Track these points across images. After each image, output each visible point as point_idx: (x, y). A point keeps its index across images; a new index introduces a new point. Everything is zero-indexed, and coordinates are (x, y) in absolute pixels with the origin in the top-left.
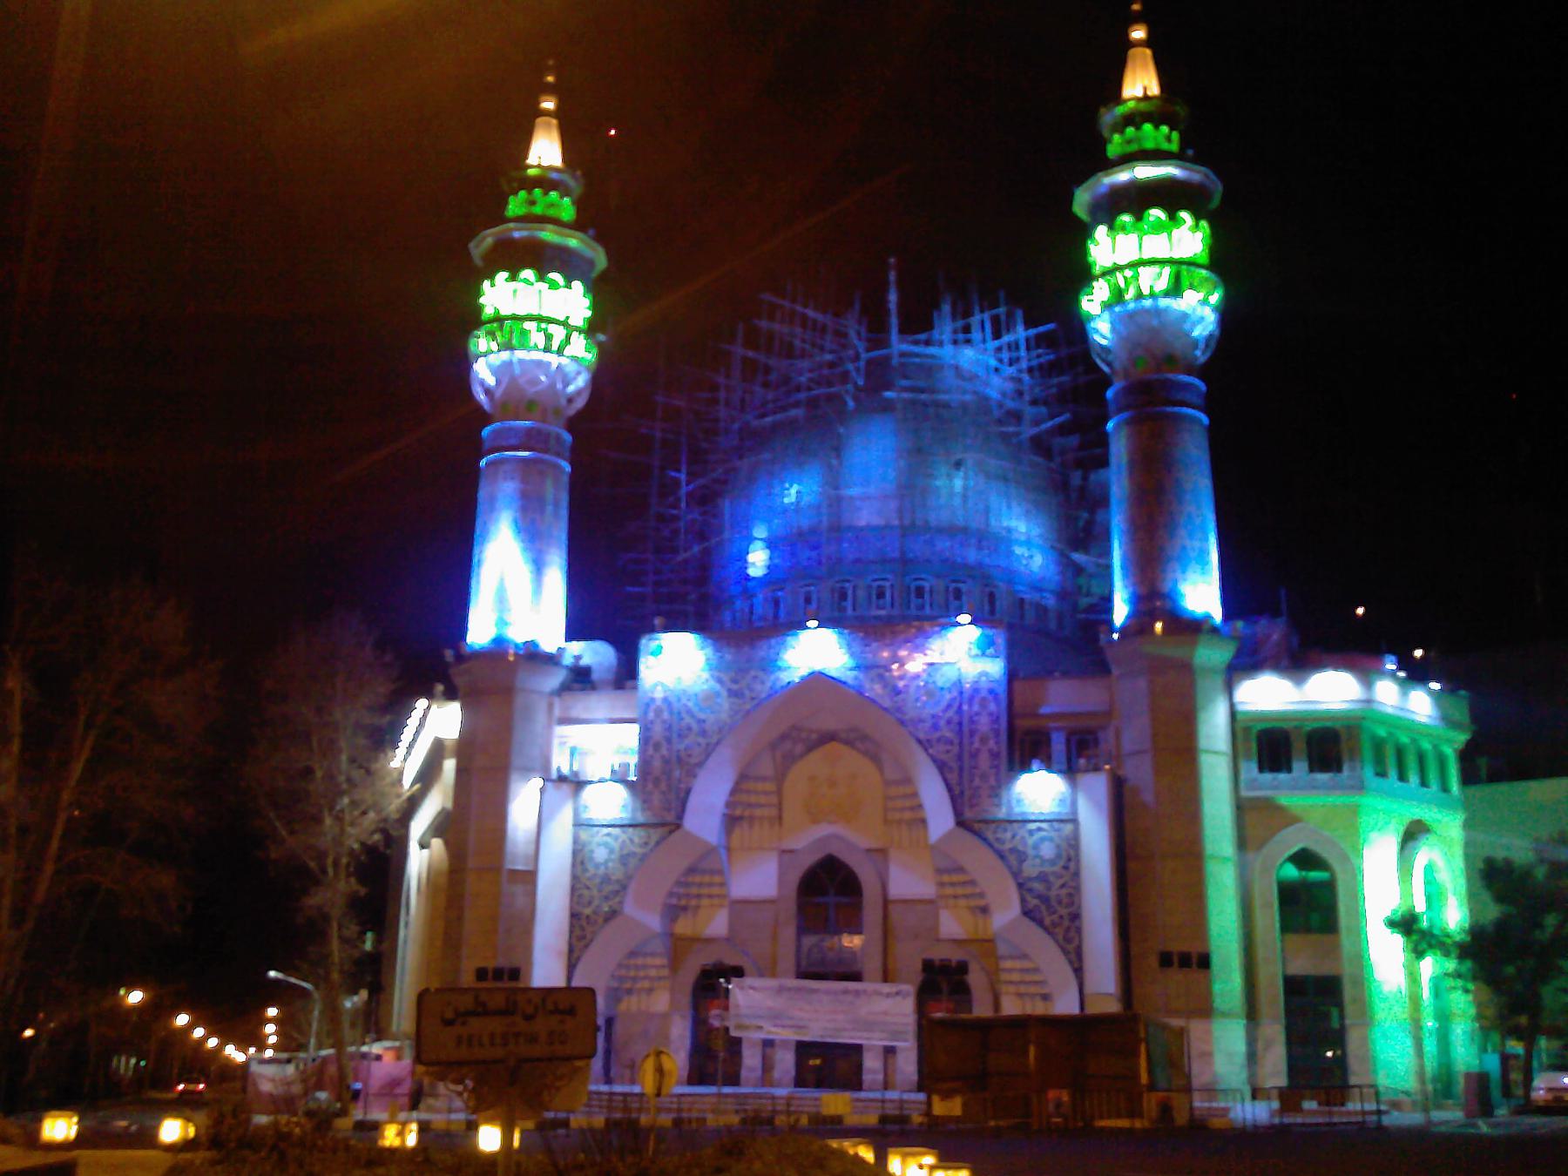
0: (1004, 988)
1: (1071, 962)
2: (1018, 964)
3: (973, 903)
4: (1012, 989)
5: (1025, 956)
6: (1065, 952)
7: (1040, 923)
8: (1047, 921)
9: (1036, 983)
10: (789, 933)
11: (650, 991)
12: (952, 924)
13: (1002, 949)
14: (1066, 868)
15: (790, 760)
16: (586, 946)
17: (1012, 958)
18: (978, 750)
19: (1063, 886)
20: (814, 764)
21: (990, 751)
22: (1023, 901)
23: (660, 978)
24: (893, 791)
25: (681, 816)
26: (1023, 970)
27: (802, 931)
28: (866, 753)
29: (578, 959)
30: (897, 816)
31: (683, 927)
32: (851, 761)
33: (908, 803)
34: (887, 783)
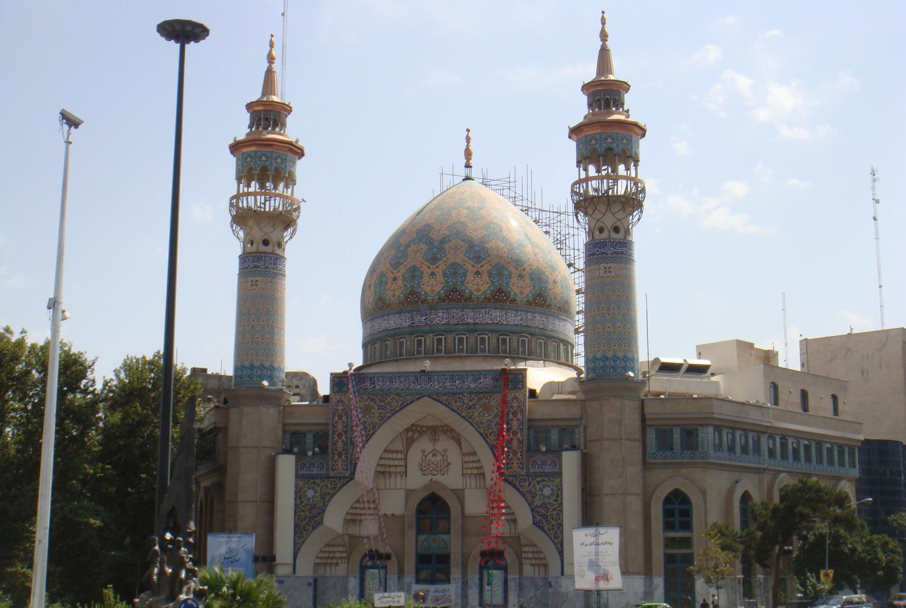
0: (524, 561)
1: (557, 549)
2: (531, 549)
3: (509, 517)
4: (528, 561)
5: (535, 545)
6: (555, 544)
7: (542, 529)
8: (546, 528)
9: (540, 559)
10: (411, 535)
11: (337, 564)
12: (500, 528)
13: (523, 541)
14: (556, 500)
15: (410, 442)
16: (303, 542)
17: (528, 546)
18: (337, 441)
19: (554, 510)
20: (424, 444)
21: (343, 441)
22: (534, 517)
23: (342, 558)
24: (467, 459)
25: (353, 474)
26: (533, 552)
27: (419, 531)
28: (453, 438)
29: (299, 549)
30: (469, 471)
31: (354, 530)
32: (445, 444)
33: (475, 465)
34: (464, 455)
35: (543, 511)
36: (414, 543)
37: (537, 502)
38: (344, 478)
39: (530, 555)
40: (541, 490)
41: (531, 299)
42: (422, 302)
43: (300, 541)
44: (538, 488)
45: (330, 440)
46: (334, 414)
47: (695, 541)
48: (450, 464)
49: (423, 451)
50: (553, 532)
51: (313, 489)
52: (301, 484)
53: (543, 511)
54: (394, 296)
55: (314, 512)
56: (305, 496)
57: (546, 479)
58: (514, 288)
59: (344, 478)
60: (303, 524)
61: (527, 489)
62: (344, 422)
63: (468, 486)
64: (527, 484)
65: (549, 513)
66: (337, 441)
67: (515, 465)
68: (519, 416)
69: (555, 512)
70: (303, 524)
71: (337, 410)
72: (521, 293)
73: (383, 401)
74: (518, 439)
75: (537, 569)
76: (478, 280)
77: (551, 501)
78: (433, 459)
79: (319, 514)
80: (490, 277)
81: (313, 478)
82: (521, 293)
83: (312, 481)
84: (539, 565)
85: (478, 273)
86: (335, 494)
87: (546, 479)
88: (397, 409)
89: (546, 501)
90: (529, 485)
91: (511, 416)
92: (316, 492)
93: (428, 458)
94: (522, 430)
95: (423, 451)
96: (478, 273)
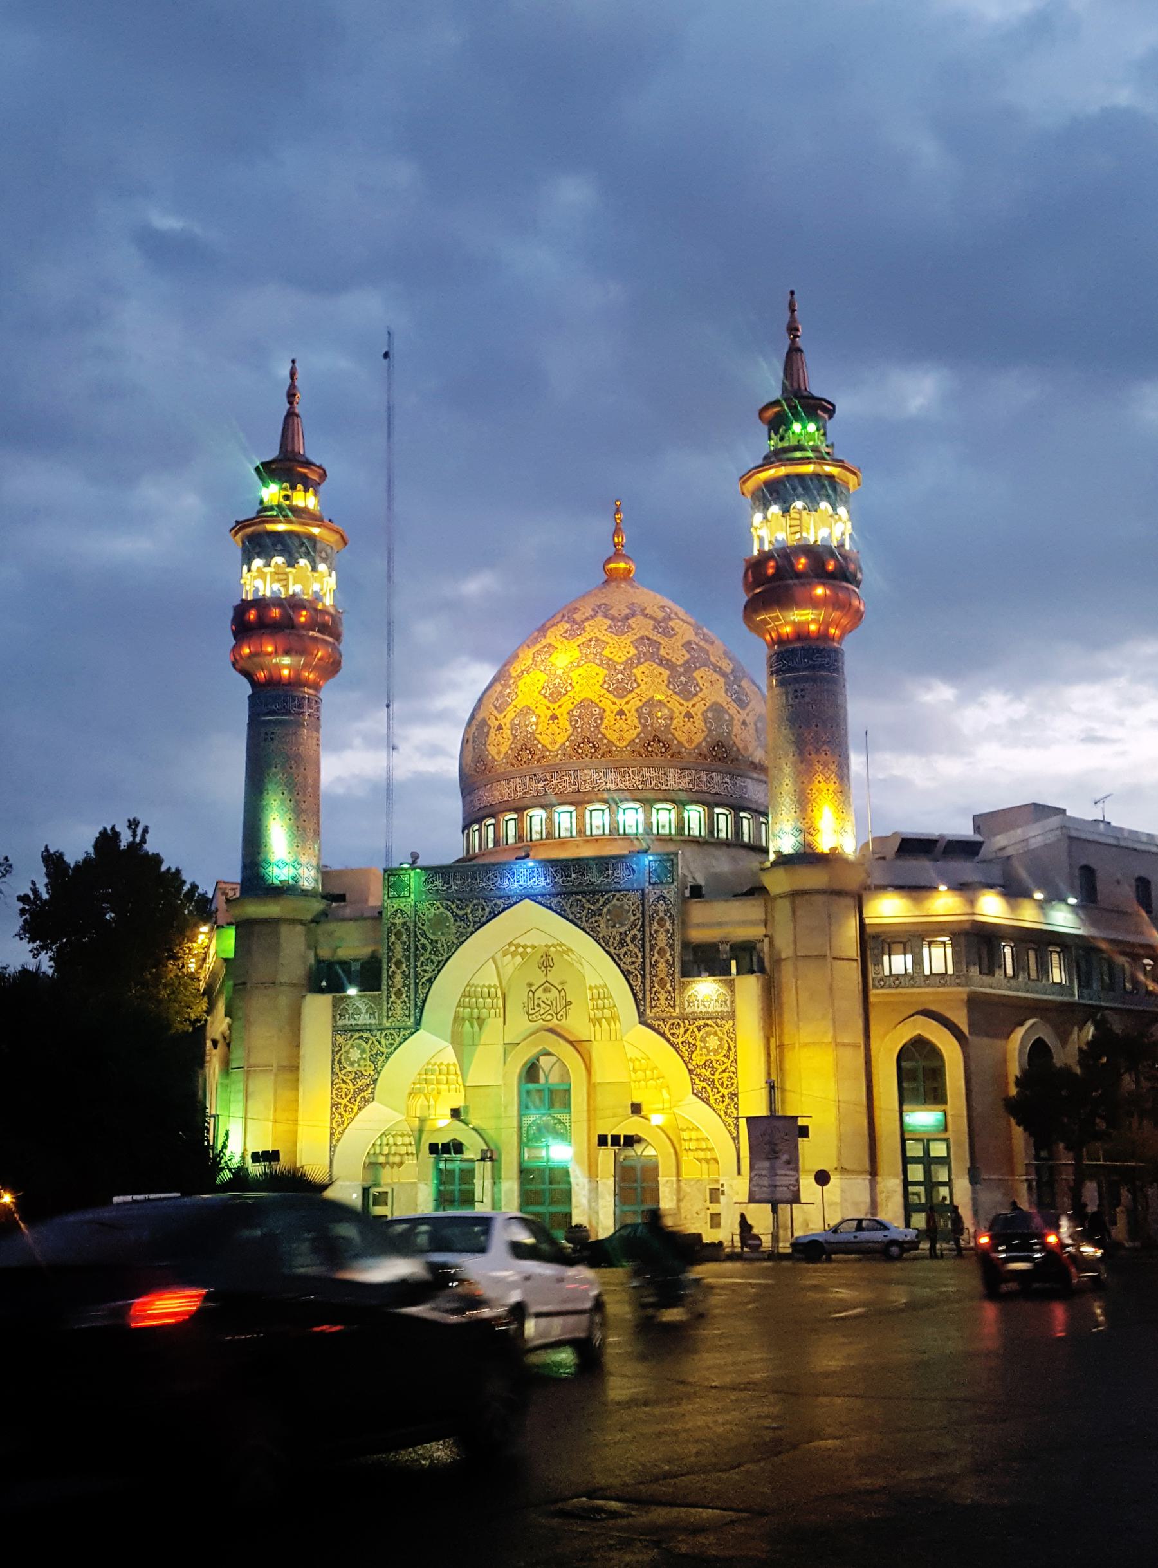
8: (712, 1102)
18: (657, 961)
21: (667, 961)
22: (693, 1083)
35: (706, 1073)
36: (515, 1124)
37: (698, 1059)
39: (693, 1145)
40: (703, 1040)
42: (732, 761)
43: (340, 1129)
45: (385, 971)
46: (390, 931)
47: (614, 1132)
49: (530, 985)
50: (722, 1106)
51: (359, 1047)
52: (340, 1039)
53: (706, 1073)
54: (499, 753)
55: (361, 1082)
56: (347, 1059)
57: (710, 1022)
60: (344, 1102)
61: (681, 1040)
63: (598, 1037)
64: (682, 1030)
65: (716, 1077)
66: (657, 961)
67: (663, 1001)
69: (726, 1075)
70: (344, 1102)
71: (394, 924)
73: (461, 909)
74: (667, 961)
75: (705, 1165)
77: (719, 1057)
78: (544, 997)
80: (639, 718)
81: (359, 1031)
83: (357, 1035)
84: (707, 1161)
85: (621, 713)
86: (392, 1053)
87: (710, 1022)
88: (484, 919)
90: (685, 1032)
91: (655, 926)
92: (364, 1051)
93: (536, 995)
94: (672, 946)
96: (621, 713)
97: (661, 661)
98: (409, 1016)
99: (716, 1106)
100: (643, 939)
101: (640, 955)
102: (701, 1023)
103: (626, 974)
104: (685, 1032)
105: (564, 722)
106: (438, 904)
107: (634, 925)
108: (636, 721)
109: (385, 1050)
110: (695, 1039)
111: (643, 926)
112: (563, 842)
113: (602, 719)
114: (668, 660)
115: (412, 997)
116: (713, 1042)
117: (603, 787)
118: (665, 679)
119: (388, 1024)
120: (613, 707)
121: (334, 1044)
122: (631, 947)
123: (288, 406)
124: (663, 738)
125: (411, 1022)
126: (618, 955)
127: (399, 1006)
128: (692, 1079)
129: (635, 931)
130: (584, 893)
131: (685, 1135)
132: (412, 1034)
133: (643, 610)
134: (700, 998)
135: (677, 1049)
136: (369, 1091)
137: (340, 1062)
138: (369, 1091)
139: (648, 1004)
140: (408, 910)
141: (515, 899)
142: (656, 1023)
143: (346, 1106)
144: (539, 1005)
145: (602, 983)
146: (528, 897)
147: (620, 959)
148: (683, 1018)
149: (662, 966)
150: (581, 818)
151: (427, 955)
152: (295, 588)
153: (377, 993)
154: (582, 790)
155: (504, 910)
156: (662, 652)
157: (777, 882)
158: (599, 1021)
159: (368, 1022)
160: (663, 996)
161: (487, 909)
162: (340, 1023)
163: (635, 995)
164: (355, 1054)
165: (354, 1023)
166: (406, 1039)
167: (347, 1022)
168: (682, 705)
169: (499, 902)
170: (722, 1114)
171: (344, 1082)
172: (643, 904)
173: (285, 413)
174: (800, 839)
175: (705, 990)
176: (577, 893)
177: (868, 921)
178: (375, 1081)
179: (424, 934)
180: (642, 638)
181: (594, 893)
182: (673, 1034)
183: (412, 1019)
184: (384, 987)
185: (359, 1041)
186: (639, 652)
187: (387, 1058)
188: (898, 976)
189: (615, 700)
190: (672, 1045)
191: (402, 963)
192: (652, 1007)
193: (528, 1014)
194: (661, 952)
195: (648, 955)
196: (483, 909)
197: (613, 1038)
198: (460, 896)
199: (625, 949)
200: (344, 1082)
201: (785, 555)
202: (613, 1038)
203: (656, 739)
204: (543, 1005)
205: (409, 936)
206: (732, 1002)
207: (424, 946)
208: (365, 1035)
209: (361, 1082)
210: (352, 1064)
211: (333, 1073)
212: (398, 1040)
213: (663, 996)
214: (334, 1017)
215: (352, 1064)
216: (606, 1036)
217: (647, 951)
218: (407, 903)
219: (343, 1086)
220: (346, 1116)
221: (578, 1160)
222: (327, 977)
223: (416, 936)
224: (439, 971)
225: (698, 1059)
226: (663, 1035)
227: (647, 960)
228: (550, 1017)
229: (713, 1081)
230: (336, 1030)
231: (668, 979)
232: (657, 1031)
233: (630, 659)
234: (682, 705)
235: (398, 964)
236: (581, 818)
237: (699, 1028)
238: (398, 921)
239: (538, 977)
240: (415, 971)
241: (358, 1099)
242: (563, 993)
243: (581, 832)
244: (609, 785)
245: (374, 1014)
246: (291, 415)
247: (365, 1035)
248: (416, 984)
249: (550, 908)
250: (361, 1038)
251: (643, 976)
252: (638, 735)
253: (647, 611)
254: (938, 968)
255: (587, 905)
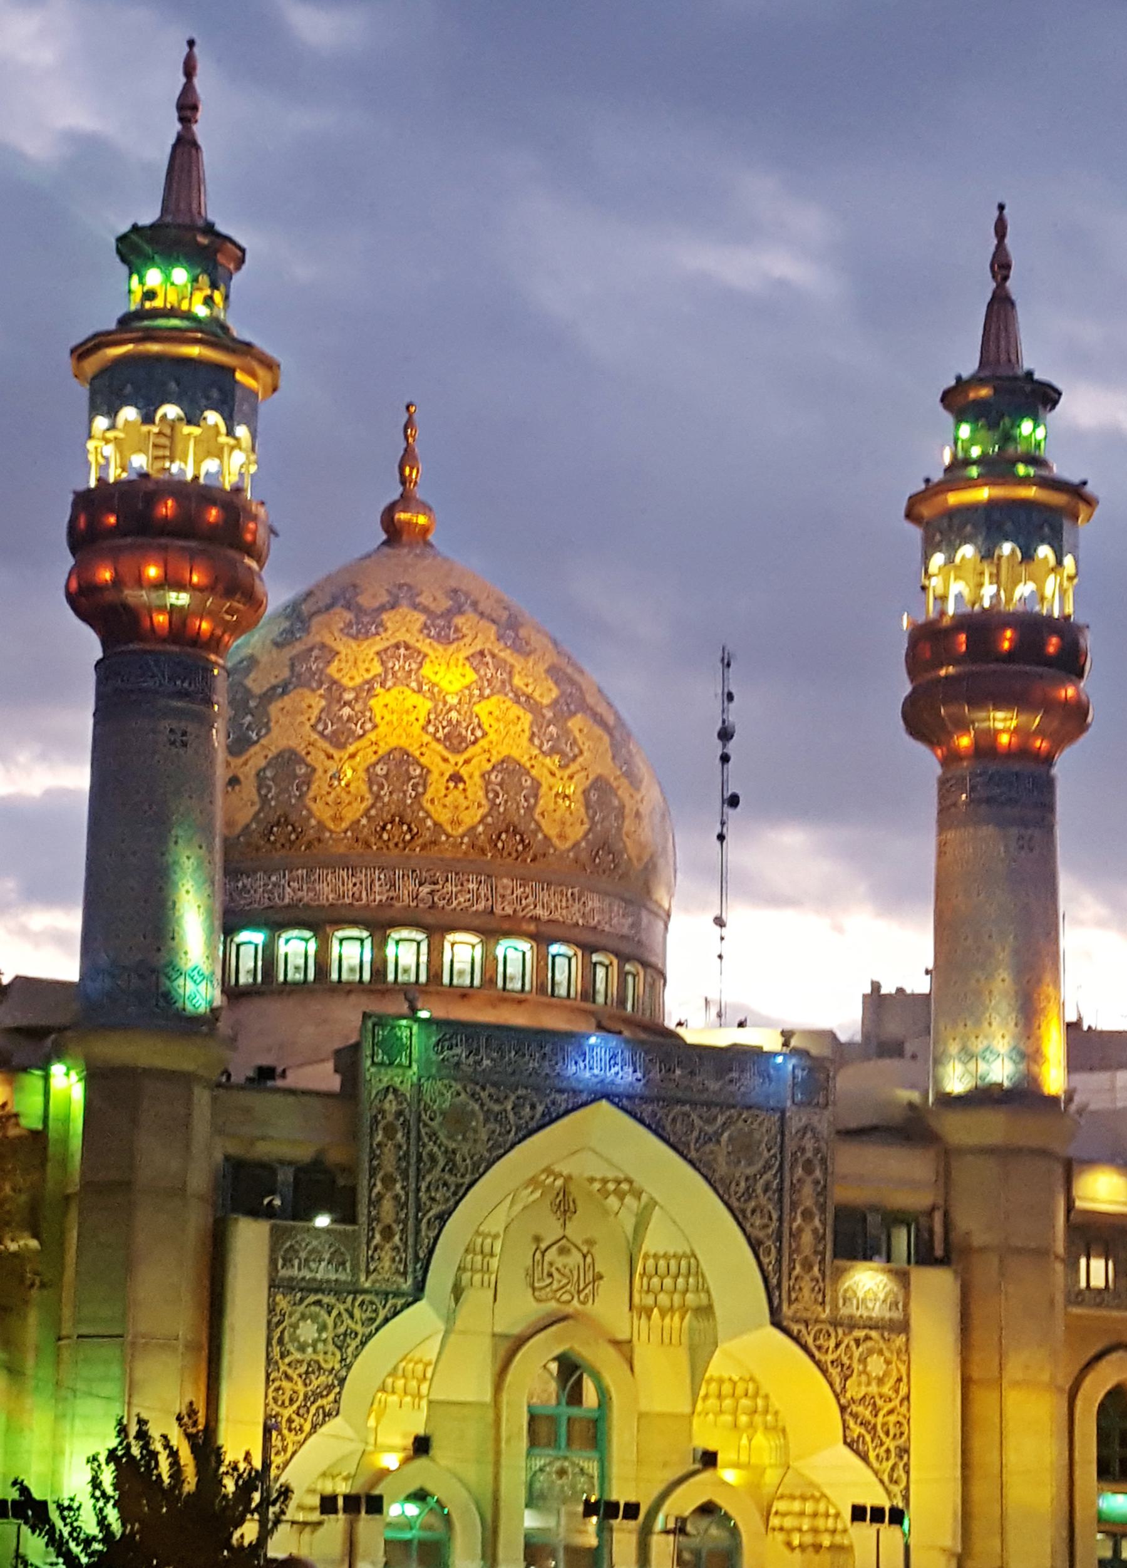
8: (872, 1455)
18: (800, 1230)
19: (891, 1412)
21: (396, 1197)
22: (845, 1427)
35: (866, 1413)
38: (397, 1294)
40: (863, 1360)
41: (584, 856)
44: (856, 1354)
46: (375, 1121)
48: (601, 1277)
51: (314, 1318)
52: (283, 1302)
55: (319, 1381)
56: (294, 1339)
58: (544, 823)
59: (397, 1294)
60: (287, 1413)
61: (830, 1357)
62: (817, 1182)
64: (832, 1343)
65: (880, 1419)
66: (800, 1230)
68: (818, 1173)
69: (892, 1419)
70: (287, 1413)
71: (382, 1111)
72: (562, 836)
73: (497, 1101)
74: (396, 1197)
76: (456, 795)
79: (330, 1388)
81: (316, 1291)
82: (562, 836)
85: (456, 778)
86: (370, 1336)
88: (533, 1125)
89: (874, 1389)
90: (837, 1346)
92: (323, 1328)
93: (547, 1258)
95: (537, 1239)
96: (456, 778)
97: (516, 695)
98: (404, 1274)
99: (876, 1465)
100: (780, 1190)
101: (775, 1216)
102: (860, 1334)
103: (755, 1245)
104: (837, 1346)
105: (475, 789)
106: (459, 1087)
107: (767, 1167)
108: (481, 793)
109: (359, 1328)
110: (850, 1358)
111: (781, 1167)
112: (506, 998)
113: (536, 796)
114: (528, 697)
115: (410, 1242)
116: (875, 1365)
117: (530, 912)
118: (527, 727)
119: (367, 1285)
120: (443, 765)
121: (271, 1310)
122: (763, 1200)
123: (178, 126)
124: (522, 828)
125: (407, 1285)
126: (743, 1211)
127: (387, 1255)
128: (844, 1421)
129: (768, 1176)
130: (694, 1104)
131: (779, 1506)
132: (408, 1305)
133: (475, 604)
134: (860, 1295)
135: (824, 1372)
136: (331, 1397)
137: (281, 1341)
138: (331, 1397)
139: (785, 1296)
140: (406, 1089)
141: (584, 1097)
142: (795, 1328)
143: (290, 1420)
144: (550, 1275)
145: (681, 1248)
146: (608, 1096)
147: (744, 1216)
148: (836, 1323)
149: (807, 1238)
150: (435, 952)
151: (437, 1172)
152: (185, 468)
153: (349, 1228)
154: (498, 910)
155: (567, 1112)
156: (517, 681)
157: (958, 1129)
158: (649, 1312)
159: (333, 1277)
160: (806, 1285)
161: (540, 1109)
162: (283, 1273)
163: (766, 1280)
164: (307, 1331)
165: (309, 1276)
166: (396, 1314)
167: (294, 1272)
168: (446, 760)
169: (561, 1098)
170: (886, 1478)
171: (288, 1378)
172: (783, 1134)
173: (172, 140)
174: (1022, 1067)
175: (868, 1283)
176: (683, 1102)
177: (1079, 1204)
178: (342, 1381)
179: (433, 1136)
180: (482, 653)
181: (709, 1104)
182: (819, 1348)
183: (410, 1281)
184: (363, 1219)
185: (316, 1309)
186: (481, 678)
187: (363, 1344)
188: (1099, 1291)
189: (446, 754)
190: (818, 1363)
191: (395, 1181)
192: (790, 1302)
193: (534, 1289)
194: (807, 1215)
195: (786, 1217)
196: (533, 1107)
197: (667, 1340)
198: (495, 1077)
199: (753, 1204)
200: (288, 1378)
201: (980, 626)
202: (667, 1340)
203: (513, 829)
204: (556, 1275)
205: (407, 1135)
206: (906, 1306)
207: (433, 1158)
208: (326, 1300)
209: (319, 1381)
210: (302, 1348)
211: (269, 1360)
212: (382, 1314)
213: (806, 1285)
214: (273, 1262)
215: (302, 1348)
216: (655, 1337)
217: (787, 1209)
218: (407, 1078)
219: (286, 1384)
220: (291, 1438)
221: (26, 1540)
222: (246, 1187)
223: (419, 1137)
224: (457, 1203)
225: (854, 1390)
226: (805, 1348)
227: (786, 1225)
228: (566, 1297)
229: (875, 1427)
230: (274, 1285)
231: (397, 1228)
232: (796, 1339)
233: (468, 687)
234: (446, 760)
235: (388, 1181)
236: (435, 952)
237: (858, 1342)
238: (391, 1106)
239: (552, 1229)
240: (418, 1199)
241: (313, 1410)
242: (589, 1260)
243: (435, 975)
244: (539, 911)
245: (343, 1264)
246: (185, 147)
247: (326, 1300)
248: (418, 1221)
249: (641, 1121)
250: (318, 1303)
251: (779, 1250)
252: (484, 818)
253: (481, 607)
254: (1098, 1281)
255: (698, 1122)
